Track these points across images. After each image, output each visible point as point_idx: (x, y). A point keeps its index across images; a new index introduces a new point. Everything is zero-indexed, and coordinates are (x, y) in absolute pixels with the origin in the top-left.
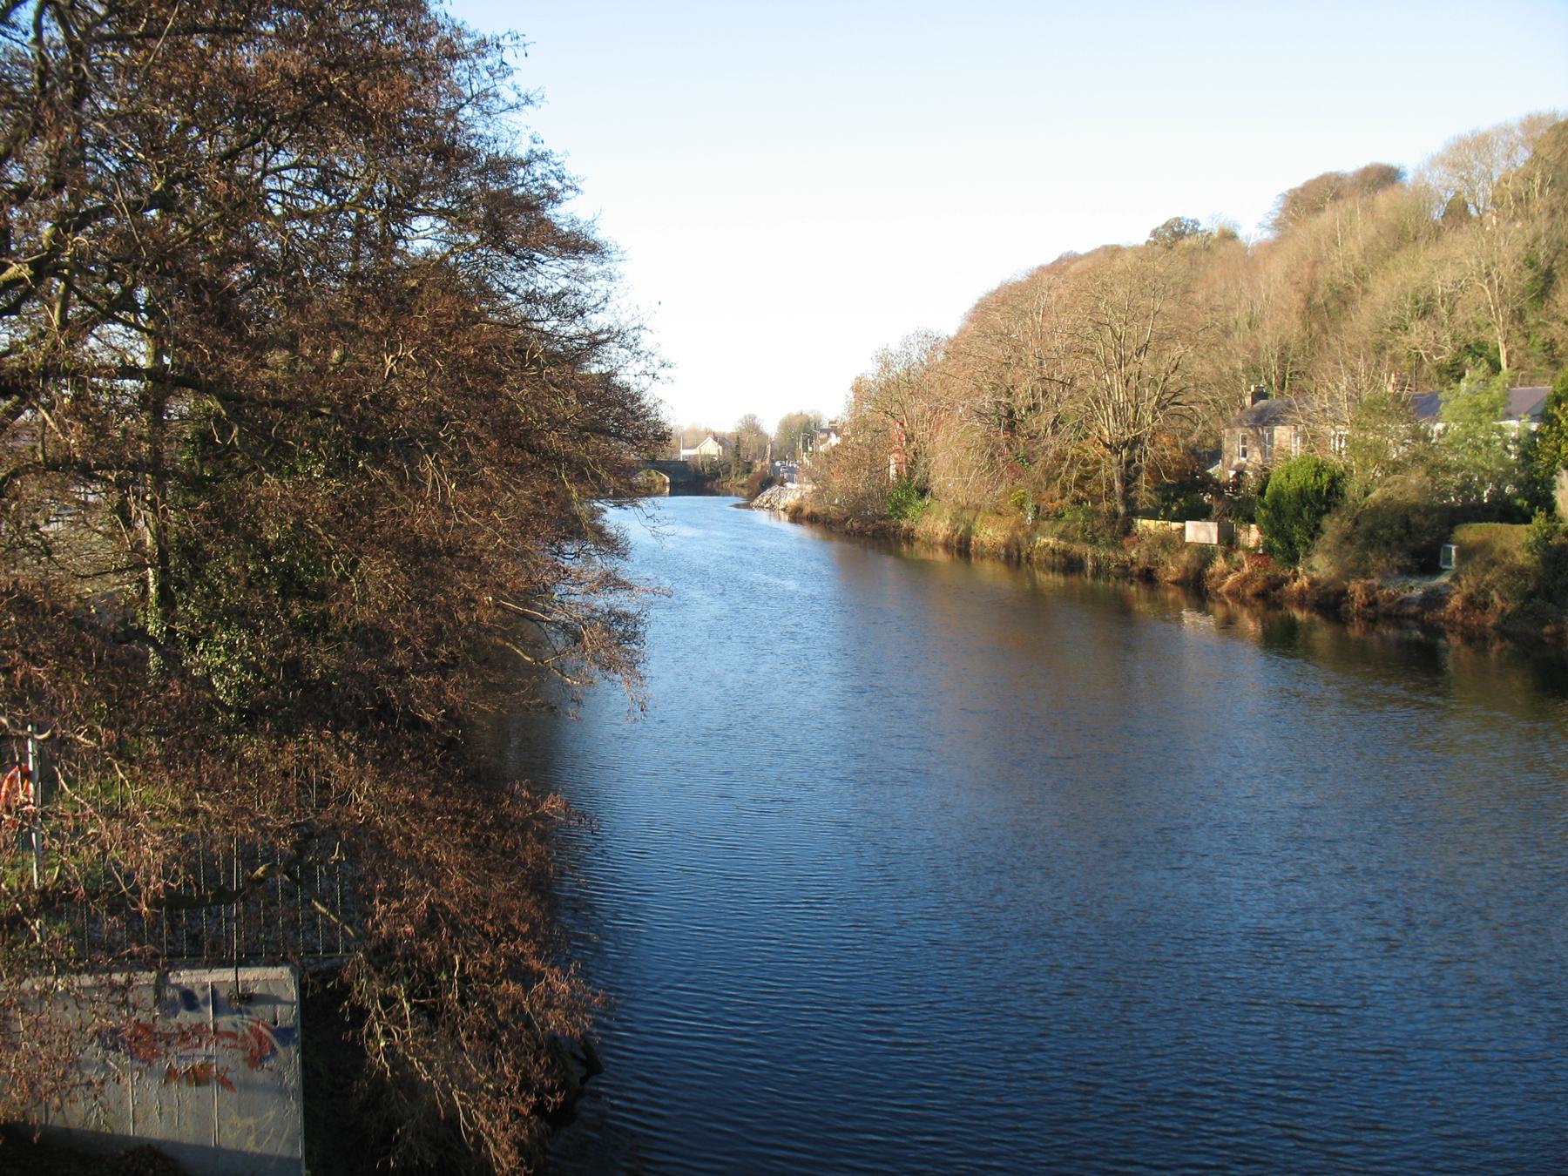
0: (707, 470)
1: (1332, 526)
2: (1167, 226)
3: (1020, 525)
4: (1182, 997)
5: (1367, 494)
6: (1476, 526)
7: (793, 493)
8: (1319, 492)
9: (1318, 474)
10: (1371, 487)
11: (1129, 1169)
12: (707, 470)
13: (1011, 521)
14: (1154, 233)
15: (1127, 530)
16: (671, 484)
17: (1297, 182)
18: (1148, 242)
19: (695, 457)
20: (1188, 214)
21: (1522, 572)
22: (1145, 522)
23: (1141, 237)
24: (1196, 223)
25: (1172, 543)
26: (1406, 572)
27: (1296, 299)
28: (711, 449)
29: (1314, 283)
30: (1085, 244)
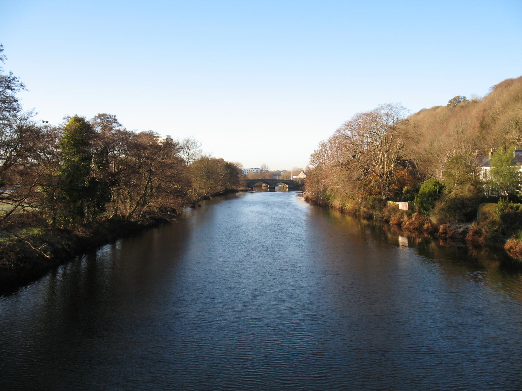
0: (300, 183)
1: (440, 205)
2: (455, 99)
3: (357, 203)
4: (213, 305)
5: (450, 192)
6: (489, 204)
7: (307, 194)
8: (435, 192)
9: (435, 185)
10: (454, 191)
11: (230, 389)
12: (300, 183)
13: (354, 201)
14: (450, 101)
15: (385, 205)
16: (289, 188)
17: (497, 82)
18: (448, 105)
19: (296, 178)
20: (462, 95)
21: (494, 223)
22: (390, 202)
23: (444, 103)
24: (464, 98)
25: (396, 209)
26: (460, 221)
27: (477, 123)
28: (302, 176)
29: (483, 118)
30: (429, 107)
